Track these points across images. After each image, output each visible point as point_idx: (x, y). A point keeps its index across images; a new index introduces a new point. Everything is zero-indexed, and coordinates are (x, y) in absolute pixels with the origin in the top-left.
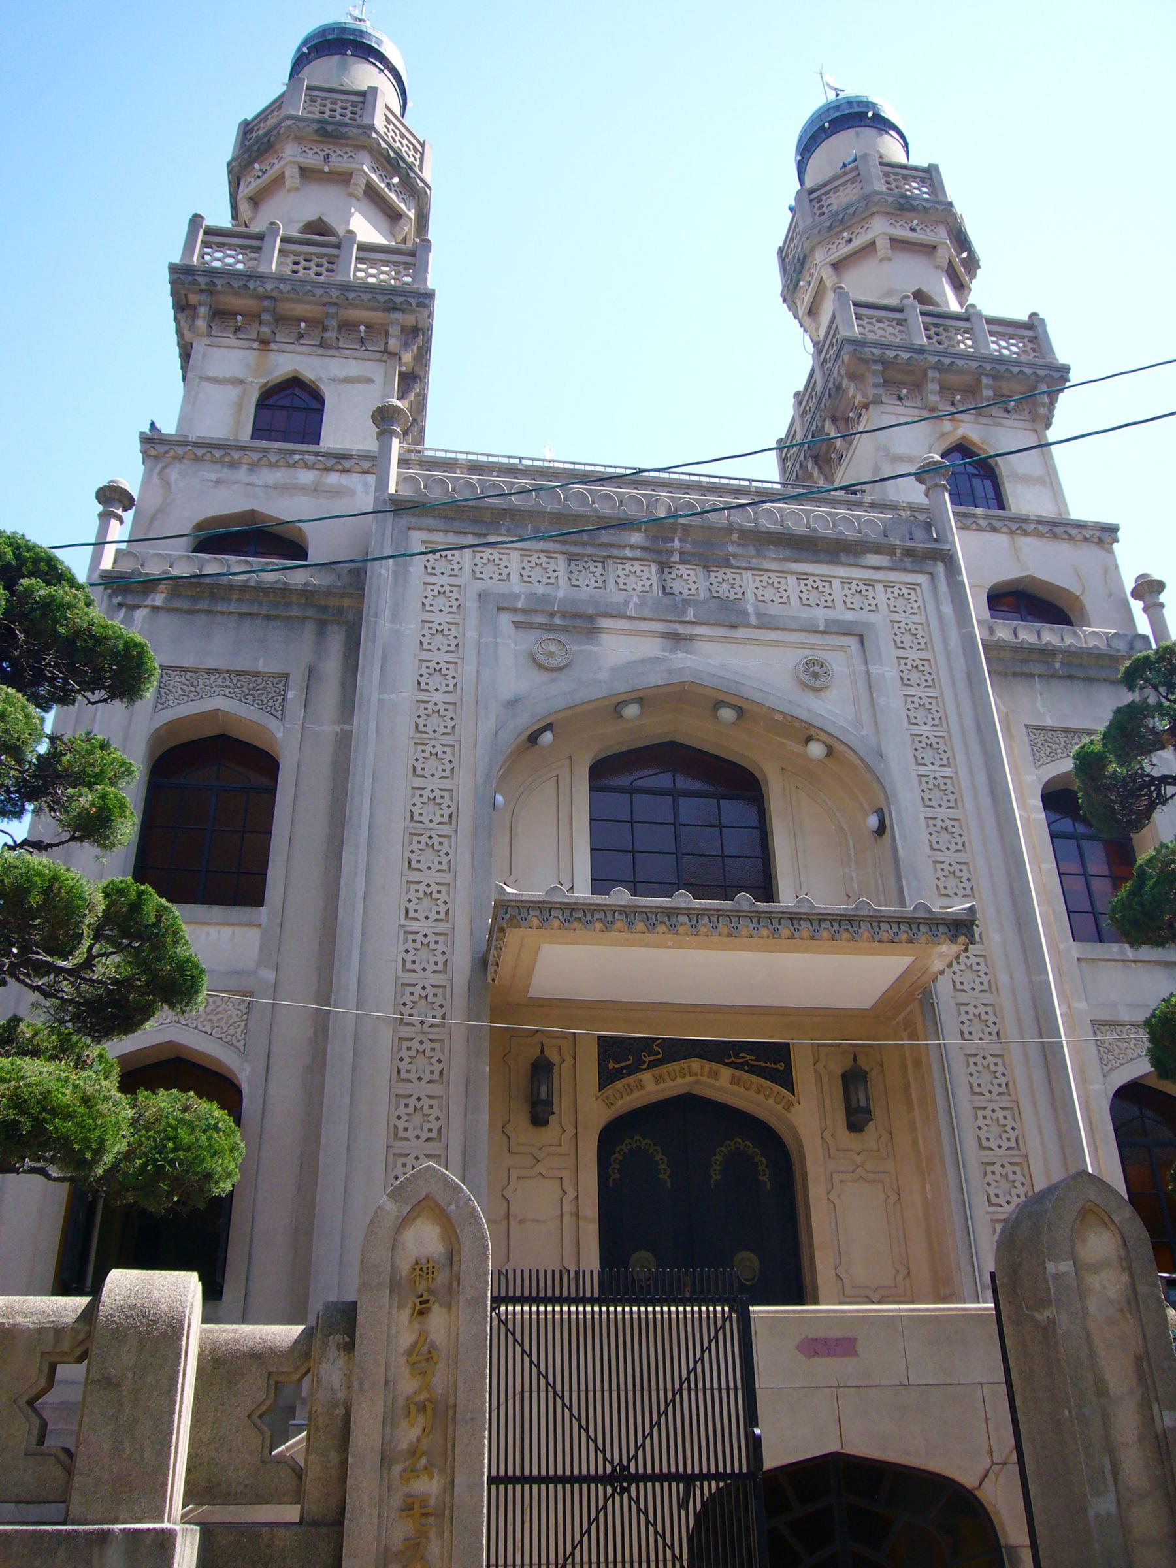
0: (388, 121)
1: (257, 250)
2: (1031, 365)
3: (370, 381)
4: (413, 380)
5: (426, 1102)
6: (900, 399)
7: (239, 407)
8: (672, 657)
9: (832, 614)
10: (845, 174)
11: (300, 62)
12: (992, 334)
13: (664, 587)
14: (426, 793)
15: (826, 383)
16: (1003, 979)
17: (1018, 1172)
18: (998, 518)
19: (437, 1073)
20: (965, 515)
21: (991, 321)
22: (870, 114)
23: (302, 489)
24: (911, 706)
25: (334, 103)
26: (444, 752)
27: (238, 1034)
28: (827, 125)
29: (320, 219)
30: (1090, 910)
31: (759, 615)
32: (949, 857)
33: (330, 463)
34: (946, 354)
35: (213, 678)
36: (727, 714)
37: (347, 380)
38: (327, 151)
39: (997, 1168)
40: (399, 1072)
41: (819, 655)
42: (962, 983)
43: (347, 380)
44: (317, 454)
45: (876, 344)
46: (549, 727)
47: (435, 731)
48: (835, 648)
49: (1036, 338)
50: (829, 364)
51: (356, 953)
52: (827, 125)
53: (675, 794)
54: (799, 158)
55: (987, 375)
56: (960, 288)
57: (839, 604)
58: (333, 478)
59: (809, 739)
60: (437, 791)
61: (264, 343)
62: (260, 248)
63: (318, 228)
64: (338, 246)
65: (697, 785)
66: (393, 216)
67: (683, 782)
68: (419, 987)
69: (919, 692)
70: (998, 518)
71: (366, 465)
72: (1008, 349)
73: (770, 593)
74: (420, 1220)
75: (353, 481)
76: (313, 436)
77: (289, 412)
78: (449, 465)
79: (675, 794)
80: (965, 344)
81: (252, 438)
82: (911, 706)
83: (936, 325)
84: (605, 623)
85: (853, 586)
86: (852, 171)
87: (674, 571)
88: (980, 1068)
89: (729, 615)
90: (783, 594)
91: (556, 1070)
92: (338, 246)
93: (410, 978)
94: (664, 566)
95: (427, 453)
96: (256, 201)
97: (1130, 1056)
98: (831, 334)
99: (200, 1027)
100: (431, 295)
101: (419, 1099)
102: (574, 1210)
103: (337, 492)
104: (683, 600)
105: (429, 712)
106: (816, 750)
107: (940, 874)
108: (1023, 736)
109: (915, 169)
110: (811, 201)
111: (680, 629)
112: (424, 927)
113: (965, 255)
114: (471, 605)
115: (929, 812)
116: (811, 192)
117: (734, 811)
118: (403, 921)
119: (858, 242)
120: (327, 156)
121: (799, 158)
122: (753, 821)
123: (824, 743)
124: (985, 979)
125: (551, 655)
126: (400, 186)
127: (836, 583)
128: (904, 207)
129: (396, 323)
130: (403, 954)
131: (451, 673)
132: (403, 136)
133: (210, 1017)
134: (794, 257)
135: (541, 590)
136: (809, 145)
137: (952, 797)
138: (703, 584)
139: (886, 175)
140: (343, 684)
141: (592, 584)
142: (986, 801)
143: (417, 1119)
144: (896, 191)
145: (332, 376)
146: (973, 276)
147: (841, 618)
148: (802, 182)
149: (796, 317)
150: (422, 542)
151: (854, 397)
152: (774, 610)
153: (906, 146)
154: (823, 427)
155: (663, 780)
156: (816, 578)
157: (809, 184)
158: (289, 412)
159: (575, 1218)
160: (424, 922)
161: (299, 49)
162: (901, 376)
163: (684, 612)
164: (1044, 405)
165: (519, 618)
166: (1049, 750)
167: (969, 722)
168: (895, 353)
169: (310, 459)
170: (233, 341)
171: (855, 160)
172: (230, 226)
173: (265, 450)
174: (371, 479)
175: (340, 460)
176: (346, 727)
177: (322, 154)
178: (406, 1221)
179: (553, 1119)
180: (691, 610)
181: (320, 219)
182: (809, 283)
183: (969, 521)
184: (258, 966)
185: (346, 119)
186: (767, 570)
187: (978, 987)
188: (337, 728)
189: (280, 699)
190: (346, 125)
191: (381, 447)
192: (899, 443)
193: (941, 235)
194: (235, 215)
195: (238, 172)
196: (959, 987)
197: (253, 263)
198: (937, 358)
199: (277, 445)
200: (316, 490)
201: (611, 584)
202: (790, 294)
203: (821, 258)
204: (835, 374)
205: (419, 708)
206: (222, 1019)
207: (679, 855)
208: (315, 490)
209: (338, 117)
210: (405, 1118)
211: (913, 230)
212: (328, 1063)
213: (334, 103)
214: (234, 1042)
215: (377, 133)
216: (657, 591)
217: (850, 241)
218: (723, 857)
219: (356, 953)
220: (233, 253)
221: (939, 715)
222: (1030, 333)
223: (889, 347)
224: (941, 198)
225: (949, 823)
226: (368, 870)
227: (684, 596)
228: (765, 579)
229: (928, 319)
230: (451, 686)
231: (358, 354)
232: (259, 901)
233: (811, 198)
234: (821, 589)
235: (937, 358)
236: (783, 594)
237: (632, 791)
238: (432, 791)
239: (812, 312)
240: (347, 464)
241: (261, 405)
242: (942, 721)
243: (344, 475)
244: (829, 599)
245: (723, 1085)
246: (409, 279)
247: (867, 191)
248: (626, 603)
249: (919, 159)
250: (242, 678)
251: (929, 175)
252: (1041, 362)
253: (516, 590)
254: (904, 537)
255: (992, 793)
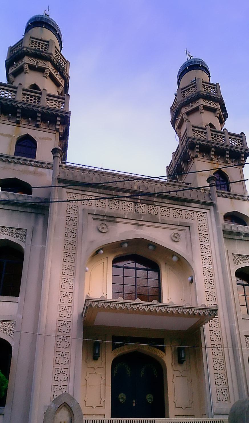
0: (56, 52)
1: (15, 92)
2: (240, 149)
3: (50, 139)
4: (64, 137)
5: (64, 354)
6: (203, 156)
7: (11, 144)
8: (137, 230)
9: (181, 220)
10: (192, 84)
11: (28, 28)
12: (230, 138)
13: (135, 210)
14: (69, 229)
15: (182, 151)
16: (222, 324)
17: (224, 376)
18: (228, 194)
19: (68, 345)
20: (219, 192)
21: (230, 134)
22: (200, 65)
23: (30, 172)
24: (202, 247)
25: (39, 44)
26: (74, 219)
27: (23, 239)
28: (187, 68)
29: (35, 84)
30: (246, 305)
31: (162, 220)
32: (210, 290)
33: (39, 165)
34: (217, 144)
35: (4, 229)
36: (151, 247)
37: (43, 139)
38: (37, 61)
39: (218, 375)
40: (57, 345)
41: (177, 232)
42: (211, 325)
43: (43, 139)
44: (35, 162)
45: (198, 140)
46: (102, 249)
47: (70, 249)
48: (182, 230)
49: (242, 140)
50: (184, 145)
51: (45, 312)
52: (187, 68)
53: (135, 269)
54: (178, 78)
55: (228, 151)
56: (222, 123)
57: (184, 217)
58: (40, 170)
59: (173, 256)
60: (63, 369)
61: (18, 123)
62: (16, 92)
63: (35, 87)
64: (41, 94)
65: (142, 267)
66: (58, 85)
67: (138, 265)
68: (219, 374)
69: (209, 278)
70: (228, 194)
71: (49, 166)
72: (234, 143)
73: (165, 213)
74: (62, 410)
75: (46, 171)
76: (33, 155)
77: (26, 147)
78: (74, 168)
79: (135, 269)
80: (222, 141)
81: (15, 155)
82: (202, 247)
83: (215, 135)
84: (118, 220)
85: (188, 212)
86: (194, 84)
87: (139, 205)
88: (217, 363)
89: (153, 220)
90: (168, 214)
91: (101, 344)
92: (41, 94)
93: (61, 319)
94: (136, 203)
95: (67, 164)
96: (16, 74)
97: (241, 263)
98: (185, 135)
99: (13, 236)
100: (70, 113)
101: (63, 353)
102: (104, 383)
103: (41, 174)
104: (141, 214)
105: (69, 231)
106: (175, 258)
107: (207, 295)
108: (231, 257)
109: (212, 84)
110: (181, 92)
111: (140, 223)
112: (65, 305)
113: (224, 113)
114: (81, 212)
115: (205, 277)
116: (182, 90)
117: (152, 274)
118: (59, 303)
119: (194, 107)
120: (37, 62)
121: (178, 78)
122: (157, 277)
123: (177, 257)
124: (218, 324)
125: (103, 228)
126: (60, 73)
127: (183, 211)
128: (208, 98)
129: (58, 121)
130: (59, 312)
131: (71, 296)
132: (60, 58)
133: (16, 234)
134: (175, 110)
135: (101, 209)
136: (182, 74)
137: (212, 274)
138: (146, 210)
139: (204, 86)
140: (43, 233)
141: (115, 208)
142: (221, 276)
143: (62, 358)
144: (206, 91)
145: (39, 137)
146: (225, 120)
147: (184, 221)
148: (179, 86)
149: (174, 128)
150: (67, 192)
151: (191, 154)
152: (166, 218)
153: (209, 77)
154: (181, 163)
155: (133, 265)
156: (178, 209)
157: (181, 87)
158: (26, 147)
159: (104, 385)
160: (65, 303)
161: (28, 23)
162: (205, 150)
163: (141, 218)
164: (243, 161)
165: (94, 217)
166: (238, 261)
167: (218, 253)
168: (203, 142)
169: (33, 163)
170: (8, 122)
171: (195, 80)
172: (6, 83)
173: (19, 159)
174: (51, 171)
175: (41, 165)
176: (44, 246)
177: (35, 61)
178: (58, 410)
179: (100, 359)
180: (143, 217)
181: (35, 84)
182: (179, 119)
183: (220, 194)
184: (17, 314)
185: (36, 104)
186: (164, 207)
187: (216, 326)
188: (41, 246)
189: (24, 236)
190: (43, 52)
191: (54, 161)
192: (202, 168)
193: (218, 106)
194: (8, 79)
195: (9, 64)
196: (212, 339)
197: (14, 97)
198: (214, 145)
199: (22, 158)
200: (34, 173)
201: (120, 208)
202: (173, 123)
203: (183, 111)
204: (185, 148)
205: (68, 207)
206: (19, 235)
207: (136, 286)
208: (34, 173)
209: (41, 49)
210: (60, 342)
211: (210, 104)
212: (42, 289)
213: (39, 44)
214: (22, 240)
215: (53, 56)
216: (133, 211)
217: (192, 106)
218: (148, 287)
219: (47, 297)
220: (7, 92)
221: (209, 250)
222: (241, 139)
223: (201, 140)
224: (219, 95)
225: (216, 332)
226: (48, 300)
227: (141, 213)
228: (164, 209)
229: (213, 133)
230: (75, 236)
231: (47, 130)
232: (18, 295)
233: (182, 91)
234: (179, 213)
235: (214, 145)
236: (168, 214)
237: (124, 267)
238: (70, 241)
239: (180, 127)
240: (44, 166)
241: (17, 144)
242: (211, 264)
243: (43, 169)
244: (181, 216)
245: (146, 348)
246: (62, 107)
247: (198, 90)
248: (125, 214)
249: (213, 81)
250: (13, 230)
251: (216, 87)
252: (243, 148)
253: (94, 209)
254: (203, 198)
255: (223, 273)
